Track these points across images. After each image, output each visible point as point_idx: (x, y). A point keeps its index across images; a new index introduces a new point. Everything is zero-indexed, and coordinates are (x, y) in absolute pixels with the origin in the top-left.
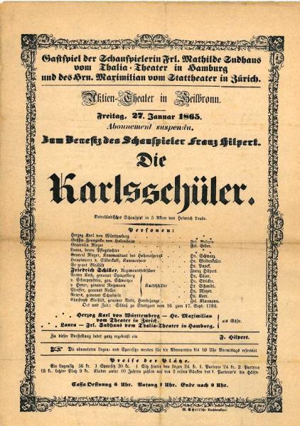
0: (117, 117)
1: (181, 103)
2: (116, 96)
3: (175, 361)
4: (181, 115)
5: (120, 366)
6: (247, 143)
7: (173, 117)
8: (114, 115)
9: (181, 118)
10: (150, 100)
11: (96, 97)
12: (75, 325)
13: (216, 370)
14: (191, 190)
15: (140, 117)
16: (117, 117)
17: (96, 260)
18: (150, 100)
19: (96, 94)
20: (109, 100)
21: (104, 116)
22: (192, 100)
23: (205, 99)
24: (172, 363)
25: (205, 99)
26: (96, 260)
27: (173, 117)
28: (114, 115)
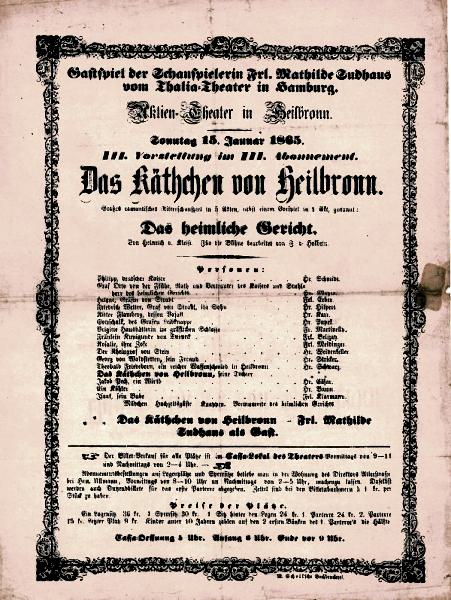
1: (273, 119)
10: (228, 115)
18: (228, 115)
19: (147, 107)
20: (168, 115)
22: (290, 115)
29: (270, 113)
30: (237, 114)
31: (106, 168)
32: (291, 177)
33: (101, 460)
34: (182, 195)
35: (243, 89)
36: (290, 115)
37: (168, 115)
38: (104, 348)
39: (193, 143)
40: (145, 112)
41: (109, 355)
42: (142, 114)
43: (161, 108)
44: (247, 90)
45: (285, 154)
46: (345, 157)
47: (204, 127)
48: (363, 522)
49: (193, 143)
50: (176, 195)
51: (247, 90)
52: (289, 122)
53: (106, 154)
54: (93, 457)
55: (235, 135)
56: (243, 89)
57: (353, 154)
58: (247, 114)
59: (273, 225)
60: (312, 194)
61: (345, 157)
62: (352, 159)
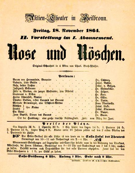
0: (45, 31)
1: (84, 21)
2: (46, 17)
3: (81, 124)
4: (87, 30)
5: (54, 127)
6: (81, 31)
7: (82, 31)
8: (43, 30)
9: (87, 31)
10: (66, 19)
11: (34, 18)
12: (109, 161)
13: (111, 129)
14: (60, 57)
15: (81, 37)
16: (45, 31)
17: (20, 91)
18: (66, 19)
19: (34, 16)
20: (42, 19)
21: (37, 30)
22: (90, 19)
23: (98, 18)
24: (80, 125)
25: (98, 18)
26: (20, 91)
27: (82, 31)
28: (43, 30)
29: (82, 18)
30: (70, 19)
31: (23, 46)
32: (57, 17)
33: (20, 137)
34: (110, 60)
35: (108, 137)
36: (90, 19)
37: (42, 19)
38: (15, 110)
39: (48, 31)
40: (33, 18)
41: (17, 113)
42: (31, 19)
43: (39, 16)
44: (82, 32)
45: (84, 37)
46: (108, 38)
47: (55, 25)
48: (79, 137)
49: (48, 31)
50: (107, 60)
51: (82, 32)
52: (90, 21)
53: (22, 37)
54: (18, 136)
55: (67, 28)
56: (108, 137)
57: (111, 37)
58: (73, 18)
59: (61, 76)
60: (18, 60)
61: (108, 38)
62: (111, 39)
